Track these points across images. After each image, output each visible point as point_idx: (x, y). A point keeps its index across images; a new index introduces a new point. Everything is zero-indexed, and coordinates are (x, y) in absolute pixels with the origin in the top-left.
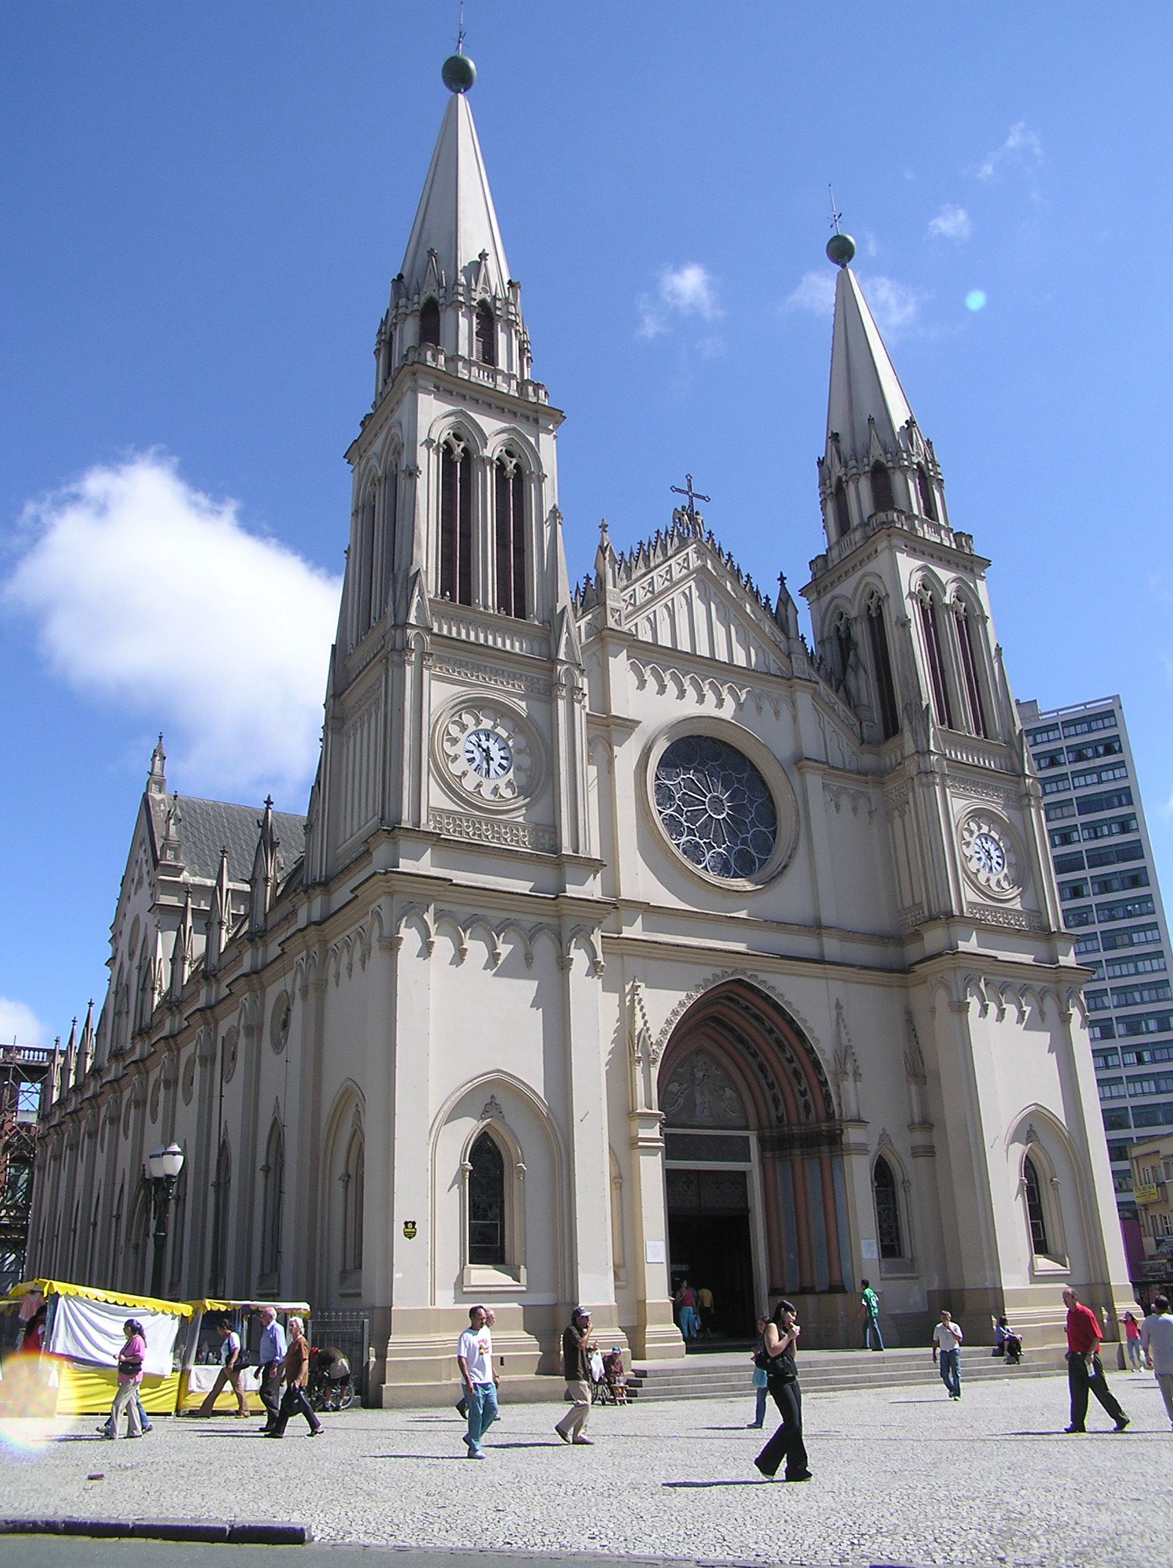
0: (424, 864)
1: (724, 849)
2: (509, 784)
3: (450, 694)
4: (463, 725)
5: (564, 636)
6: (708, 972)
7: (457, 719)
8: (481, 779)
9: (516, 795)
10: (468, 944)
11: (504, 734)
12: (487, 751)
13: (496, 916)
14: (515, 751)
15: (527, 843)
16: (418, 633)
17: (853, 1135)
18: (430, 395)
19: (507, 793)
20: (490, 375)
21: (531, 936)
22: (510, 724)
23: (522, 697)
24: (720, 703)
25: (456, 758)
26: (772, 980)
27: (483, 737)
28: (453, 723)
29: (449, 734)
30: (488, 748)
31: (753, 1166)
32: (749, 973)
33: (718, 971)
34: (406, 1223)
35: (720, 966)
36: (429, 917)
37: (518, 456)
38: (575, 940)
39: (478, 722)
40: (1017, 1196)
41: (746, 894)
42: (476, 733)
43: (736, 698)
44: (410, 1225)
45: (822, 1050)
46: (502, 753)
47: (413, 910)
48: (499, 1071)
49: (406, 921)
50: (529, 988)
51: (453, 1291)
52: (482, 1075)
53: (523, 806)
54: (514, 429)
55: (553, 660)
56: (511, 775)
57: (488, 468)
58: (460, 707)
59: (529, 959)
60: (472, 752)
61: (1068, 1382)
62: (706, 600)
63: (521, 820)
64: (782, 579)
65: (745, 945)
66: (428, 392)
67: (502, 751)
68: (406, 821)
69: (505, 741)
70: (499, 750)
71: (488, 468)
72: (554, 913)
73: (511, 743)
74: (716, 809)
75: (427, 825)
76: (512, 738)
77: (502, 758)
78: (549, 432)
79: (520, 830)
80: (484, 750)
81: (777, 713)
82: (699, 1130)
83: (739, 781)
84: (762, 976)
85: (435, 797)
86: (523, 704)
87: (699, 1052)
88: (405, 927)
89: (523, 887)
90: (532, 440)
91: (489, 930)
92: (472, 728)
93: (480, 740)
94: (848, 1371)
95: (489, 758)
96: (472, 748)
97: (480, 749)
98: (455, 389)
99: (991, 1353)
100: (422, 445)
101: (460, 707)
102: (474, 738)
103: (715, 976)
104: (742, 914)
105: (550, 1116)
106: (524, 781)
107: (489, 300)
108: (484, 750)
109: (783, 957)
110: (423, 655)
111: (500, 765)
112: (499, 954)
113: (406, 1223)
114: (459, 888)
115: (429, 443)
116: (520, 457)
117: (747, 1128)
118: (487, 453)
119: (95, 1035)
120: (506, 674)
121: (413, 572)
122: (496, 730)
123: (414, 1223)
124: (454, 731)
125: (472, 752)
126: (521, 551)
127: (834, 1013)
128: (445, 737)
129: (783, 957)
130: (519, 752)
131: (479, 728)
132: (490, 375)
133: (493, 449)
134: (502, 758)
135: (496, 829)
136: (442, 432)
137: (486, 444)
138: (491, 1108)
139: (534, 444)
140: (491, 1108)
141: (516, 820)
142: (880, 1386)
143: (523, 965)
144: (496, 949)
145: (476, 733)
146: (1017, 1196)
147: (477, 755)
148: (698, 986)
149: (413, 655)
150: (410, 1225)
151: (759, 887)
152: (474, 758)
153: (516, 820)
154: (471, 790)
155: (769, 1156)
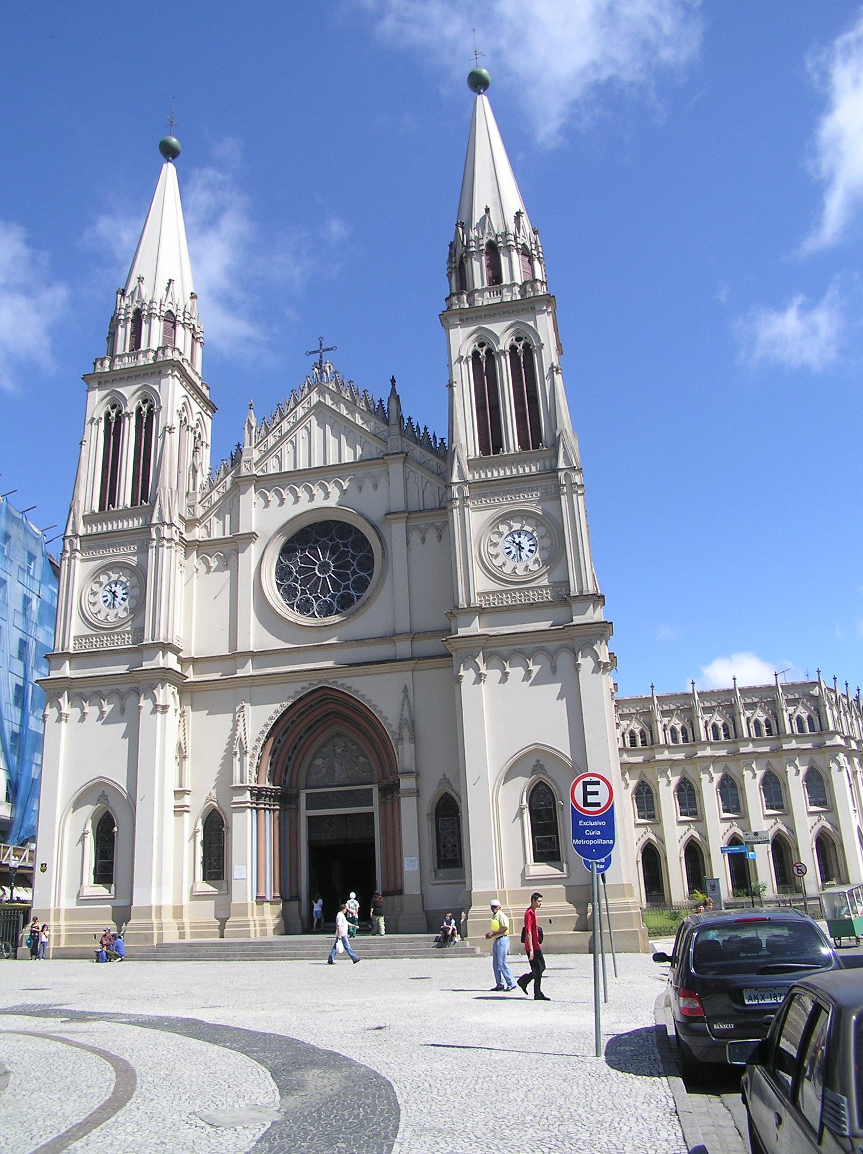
0: (476, 627)
1: (329, 597)
2: (536, 561)
3: (488, 517)
4: (500, 532)
5: (456, 464)
6: (298, 687)
7: (496, 530)
8: (515, 564)
9: (541, 566)
10: (87, 709)
11: (529, 529)
12: (519, 544)
13: (528, 648)
14: (539, 539)
15: (549, 598)
16: (566, 473)
17: (406, 783)
18: (457, 327)
19: (535, 567)
20: (498, 292)
21: (552, 656)
22: (533, 522)
23: (134, 554)
24: (327, 495)
25: (497, 556)
26: (348, 682)
27: (516, 536)
28: (493, 533)
29: (491, 541)
30: (520, 542)
31: (375, 808)
32: (330, 681)
33: (306, 684)
34: (42, 865)
35: (306, 681)
36: (479, 660)
37: (524, 338)
38: (580, 652)
39: (511, 527)
40: (79, 842)
41: (333, 626)
42: (109, 584)
43: (340, 486)
44: (44, 866)
45: (390, 725)
46: (531, 542)
47: (469, 659)
48: (101, 777)
49: (464, 666)
50: (122, 727)
51: (76, 899)
52: (527, 747)
53: (130, 620)
54: (517, 323)
55: (556, 470)
56: (537, 555)
57: (502, 357)
58: (98, 573)
59: (554, 670)
60: (510, 548)
61: (492, 960)
62: (321, 425)
63: (129, 628)
64: (393, 381)
65: (333, 662)
66: (456, 326)
67: (530, 541)
68: (462, 603)
69: (125, 583)
70: (528, 541)
71: (502, 357)
72: (568, 637)
73: (535, 534)
74: (324, 570)
75: (476, 601)
76: (535, 530)
77: (530, 545)
78: (543, 312)
79: (491, 596)
80: (517, 544)
81: (375, 487)
82: (350, 787)
83: (345, 545)
84: (340, 681)
85: (481, 583)
86: (135, 558)
87: (339, 735)
88: (582, 657)
89: (545, 625)
90: (531, 323)
91: (96, 697)
92: (506, 532)
93: (514, 539)
94: (290, 949)
95: (520, 548)
96: (106, 593)
97: (515, 544)
98: (118, 377)
99: (434, 939)
100: (455, 363)
101: (98, 573)
102: (510, 538)
103: (303, 688)
104: (333, 641)
105: (129, 799)
106: (546, 554)
107: (493, 239)
108: (517, 544)
109: (351, 665)
110: (464, 499)
111: (530, 551)
112: (105, 711)
113: (42, 865)
114: (598, 625)
115: (460, 359)
116: (526, 338)
117: (371, 783)
118: (501, 347)
119: (841, 712)
120: (514, 491)
121: (557, 434)
122: (120, 579)
123: (46, 864)
124: (495, 538)
125: (510, 548)
126: (533, 400)
127: (402, 696)
128: (489, 544)
129: (351, 665)
130: (133, 587)
131: (512, 530)
132: (498, 292)
133: (504, 343)
134: (530, 545)
135: (500, 597)
136: (467, 350)
137: (499, 341)
138: (538, 768)
139: (533, 327)
140: (103, 798)
141: (126, 629)
142: (208, 960)
143: (550, 674)
144: (480, 670)
145: (511, 534)
146: (79, 842)
147: (513, 549)
148: (289, 698)
149: (565, 488)
150: (44, 866)
151: (345, 618)
152: (511, 551)
153: (126, 629)
154: (509, 572)
155: (293, 807)
